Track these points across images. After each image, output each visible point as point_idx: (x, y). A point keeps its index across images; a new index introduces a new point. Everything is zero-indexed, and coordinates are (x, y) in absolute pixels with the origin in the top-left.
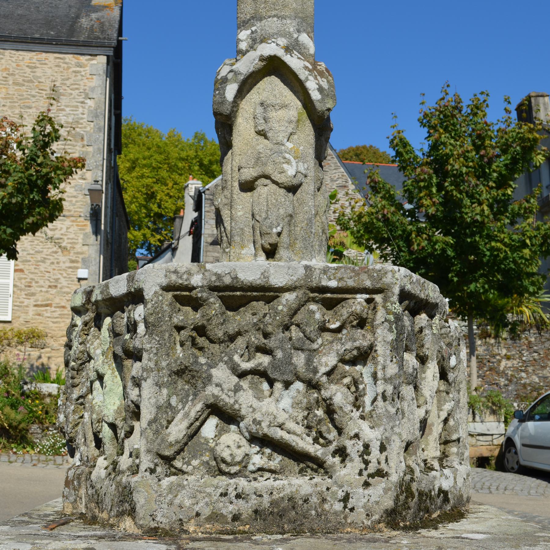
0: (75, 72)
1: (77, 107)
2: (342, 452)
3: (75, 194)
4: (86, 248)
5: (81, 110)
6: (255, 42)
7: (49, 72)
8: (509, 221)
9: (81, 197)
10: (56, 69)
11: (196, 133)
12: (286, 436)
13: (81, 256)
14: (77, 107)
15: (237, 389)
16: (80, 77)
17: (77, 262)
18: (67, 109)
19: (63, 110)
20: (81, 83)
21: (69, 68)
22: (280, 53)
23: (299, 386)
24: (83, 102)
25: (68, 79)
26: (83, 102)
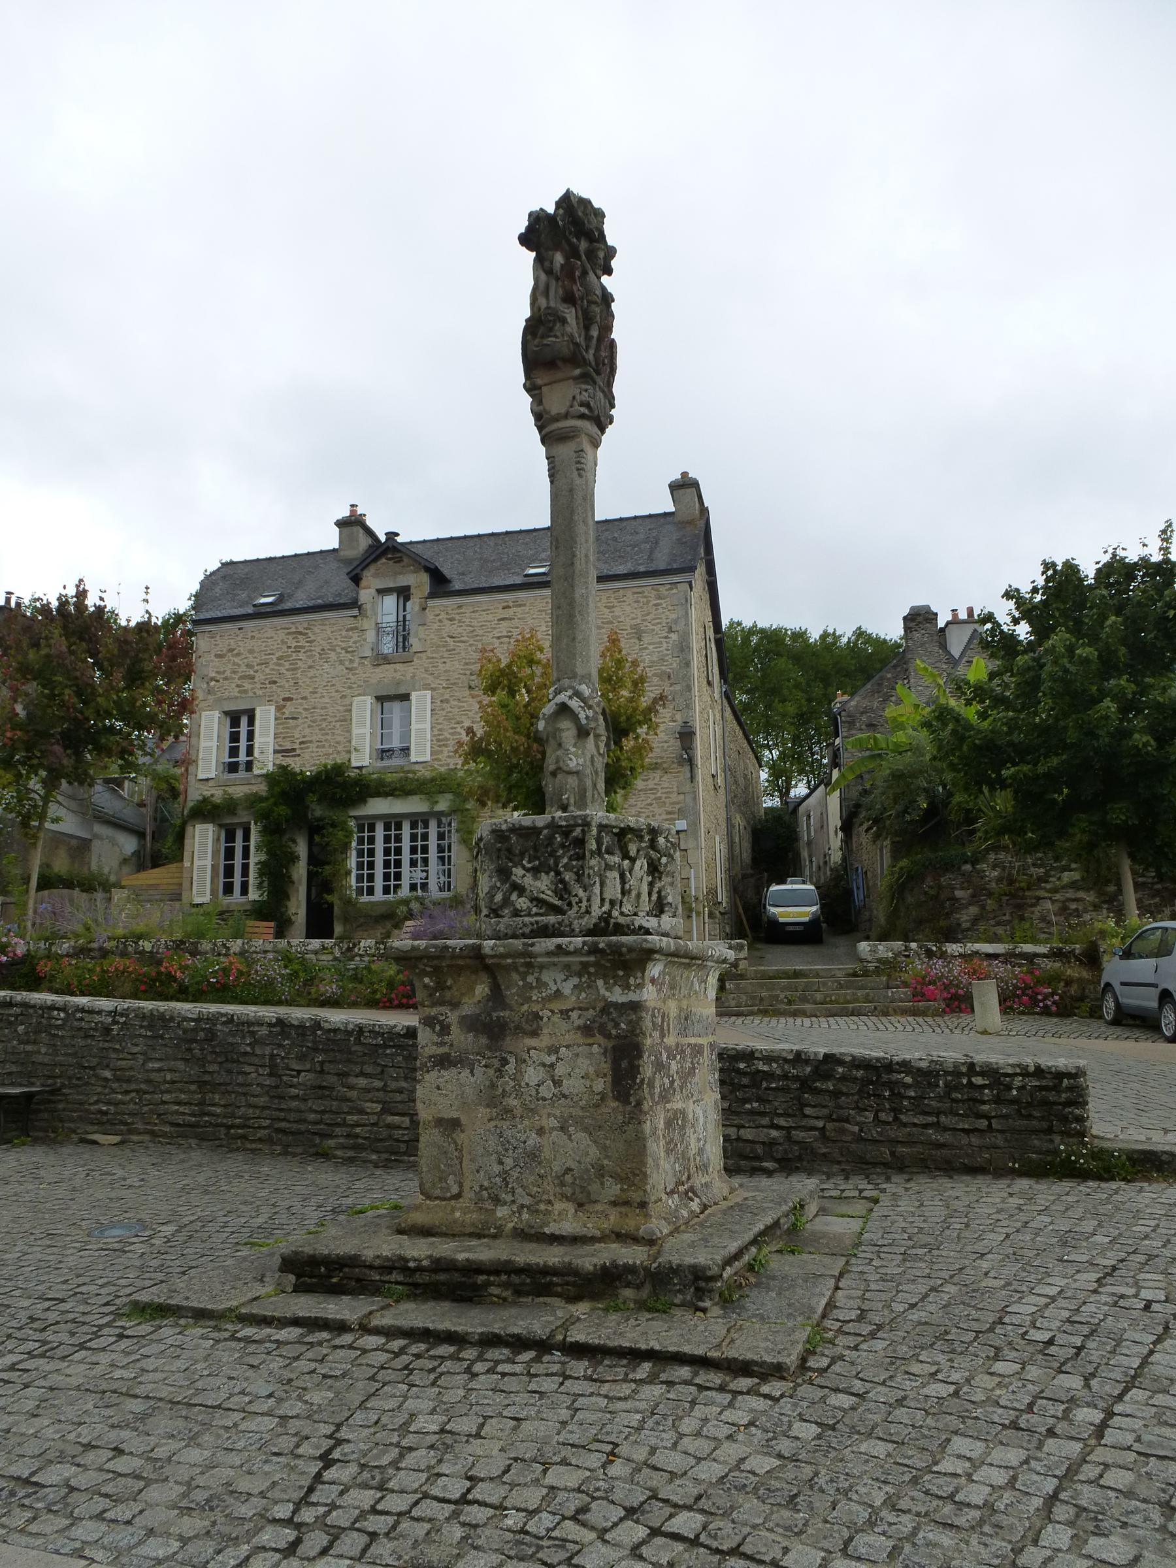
0: (655, 605)
1: (661, 643)
2: (570, 904)
3: (666, 738)
4: (682, 797)
5: (665, 645)
6: (557, 693)
7: (628, 609)
8: (129, 844)
9: (672, 741)
10: (636, 605)
11: (860, 628)
12: (544, 897)
13: (678, 806)
14: (661, 643)
15: (524, 876)
16: (661, 611)
17: (674, 813)
18: (651, 647)
19: (646, 648)
20: (663, 616)
21: (648, 602)
22: (566, 700)
23: (552, 873)
24: (666, 637)
25: (648, 614)
26: (666, 637)
